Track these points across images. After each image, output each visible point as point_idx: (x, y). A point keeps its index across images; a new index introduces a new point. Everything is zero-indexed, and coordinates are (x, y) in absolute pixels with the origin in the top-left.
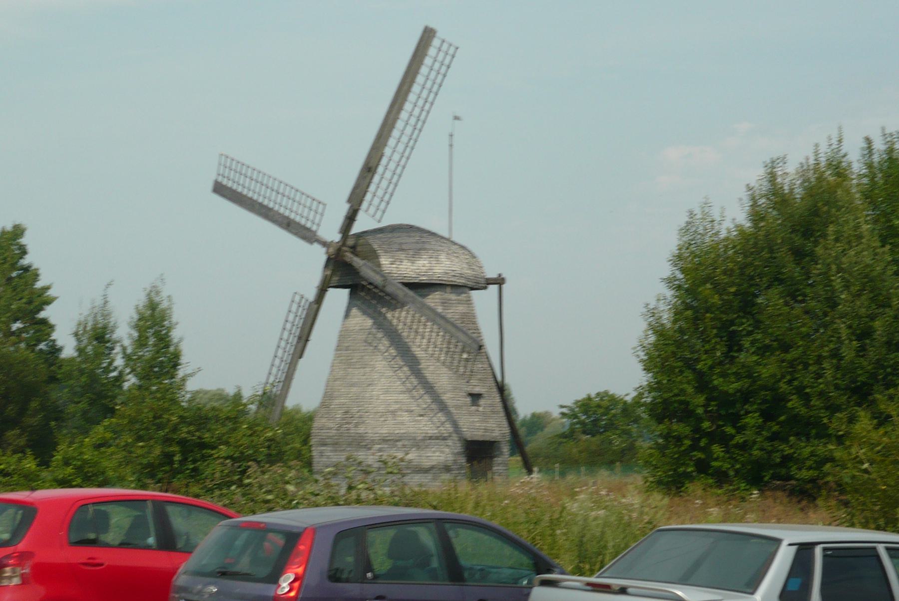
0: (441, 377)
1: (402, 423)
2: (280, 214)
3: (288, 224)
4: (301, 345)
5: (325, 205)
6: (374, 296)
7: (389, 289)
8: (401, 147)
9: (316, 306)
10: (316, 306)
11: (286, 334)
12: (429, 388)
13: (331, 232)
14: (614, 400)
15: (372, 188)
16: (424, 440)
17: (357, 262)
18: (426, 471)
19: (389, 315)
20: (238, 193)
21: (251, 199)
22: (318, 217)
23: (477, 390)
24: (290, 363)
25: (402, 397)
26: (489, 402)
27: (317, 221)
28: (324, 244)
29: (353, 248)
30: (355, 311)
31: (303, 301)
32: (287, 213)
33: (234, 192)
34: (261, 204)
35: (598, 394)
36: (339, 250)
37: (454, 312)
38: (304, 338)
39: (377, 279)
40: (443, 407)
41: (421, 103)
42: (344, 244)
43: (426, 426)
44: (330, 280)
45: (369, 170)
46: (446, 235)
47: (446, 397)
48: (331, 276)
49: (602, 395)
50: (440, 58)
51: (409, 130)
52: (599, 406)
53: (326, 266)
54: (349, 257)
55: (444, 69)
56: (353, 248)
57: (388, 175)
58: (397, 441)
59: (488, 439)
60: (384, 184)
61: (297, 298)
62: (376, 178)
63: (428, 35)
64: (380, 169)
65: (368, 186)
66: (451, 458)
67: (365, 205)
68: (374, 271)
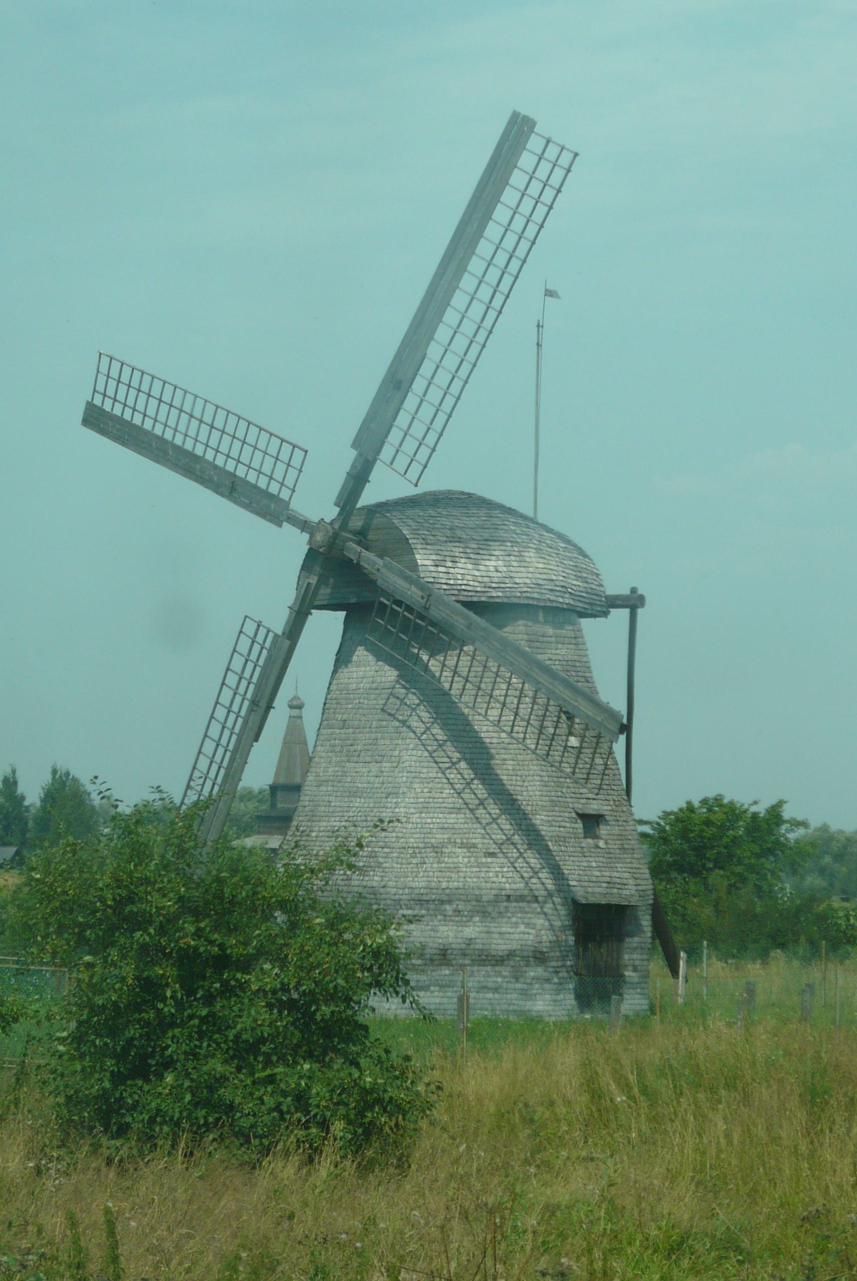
0: (528, 779)
1: (456, 869)
2: (216, 467)
3: (232, 488)
4: (255, 718)
6: (406, 626)
7: (435, 613)
8: (460, 343)
9: (287, 643)
10: (287, 643)
11: (227, 694)
12: (509, 803)
13: (319, 503)
14: (733, 813)
15: (403, 419)
16: (496, 900)
17: (370, 560)
18: (499, 961)
19: (434, 666)
21: (161, 439)
23: (594, 807)
24: (234, 752)
25: (452, 818)
26: (616, 830)
27: (289, 482)
28: (304, 525)
29: (361, 536)
30: (361, 653)
31: (262, 631)
32: (230, 466)
34: (180, 450)
35: (704, 802)
36: (336, 536)
37: (556, 655)
38: (262, 704)
39: (413, 594)
40: (534, 839)
41: (501, 259)
42: (344, 526)
43: (501, 875)
44: (315, 594)
46: (531, 514)
47: (539, 820)
48: (318, 587)
49: (713, 804)
50: (542, 173)
51: (477, 310)
52: (708, 823)
53: (307, 566)
54: (353, 550)
55: (549, 194)
56: (361, 536)
57: (434, 395)
58: (442, 902)
59: (614, 901)
60: (426, 412)
61: (250, 628)
62: (411, 402)
63: (519, 129)
64: (419, 385)
65: (395, 417)
66: (547, 937)
67: (387, 453)
68: (406, 578)
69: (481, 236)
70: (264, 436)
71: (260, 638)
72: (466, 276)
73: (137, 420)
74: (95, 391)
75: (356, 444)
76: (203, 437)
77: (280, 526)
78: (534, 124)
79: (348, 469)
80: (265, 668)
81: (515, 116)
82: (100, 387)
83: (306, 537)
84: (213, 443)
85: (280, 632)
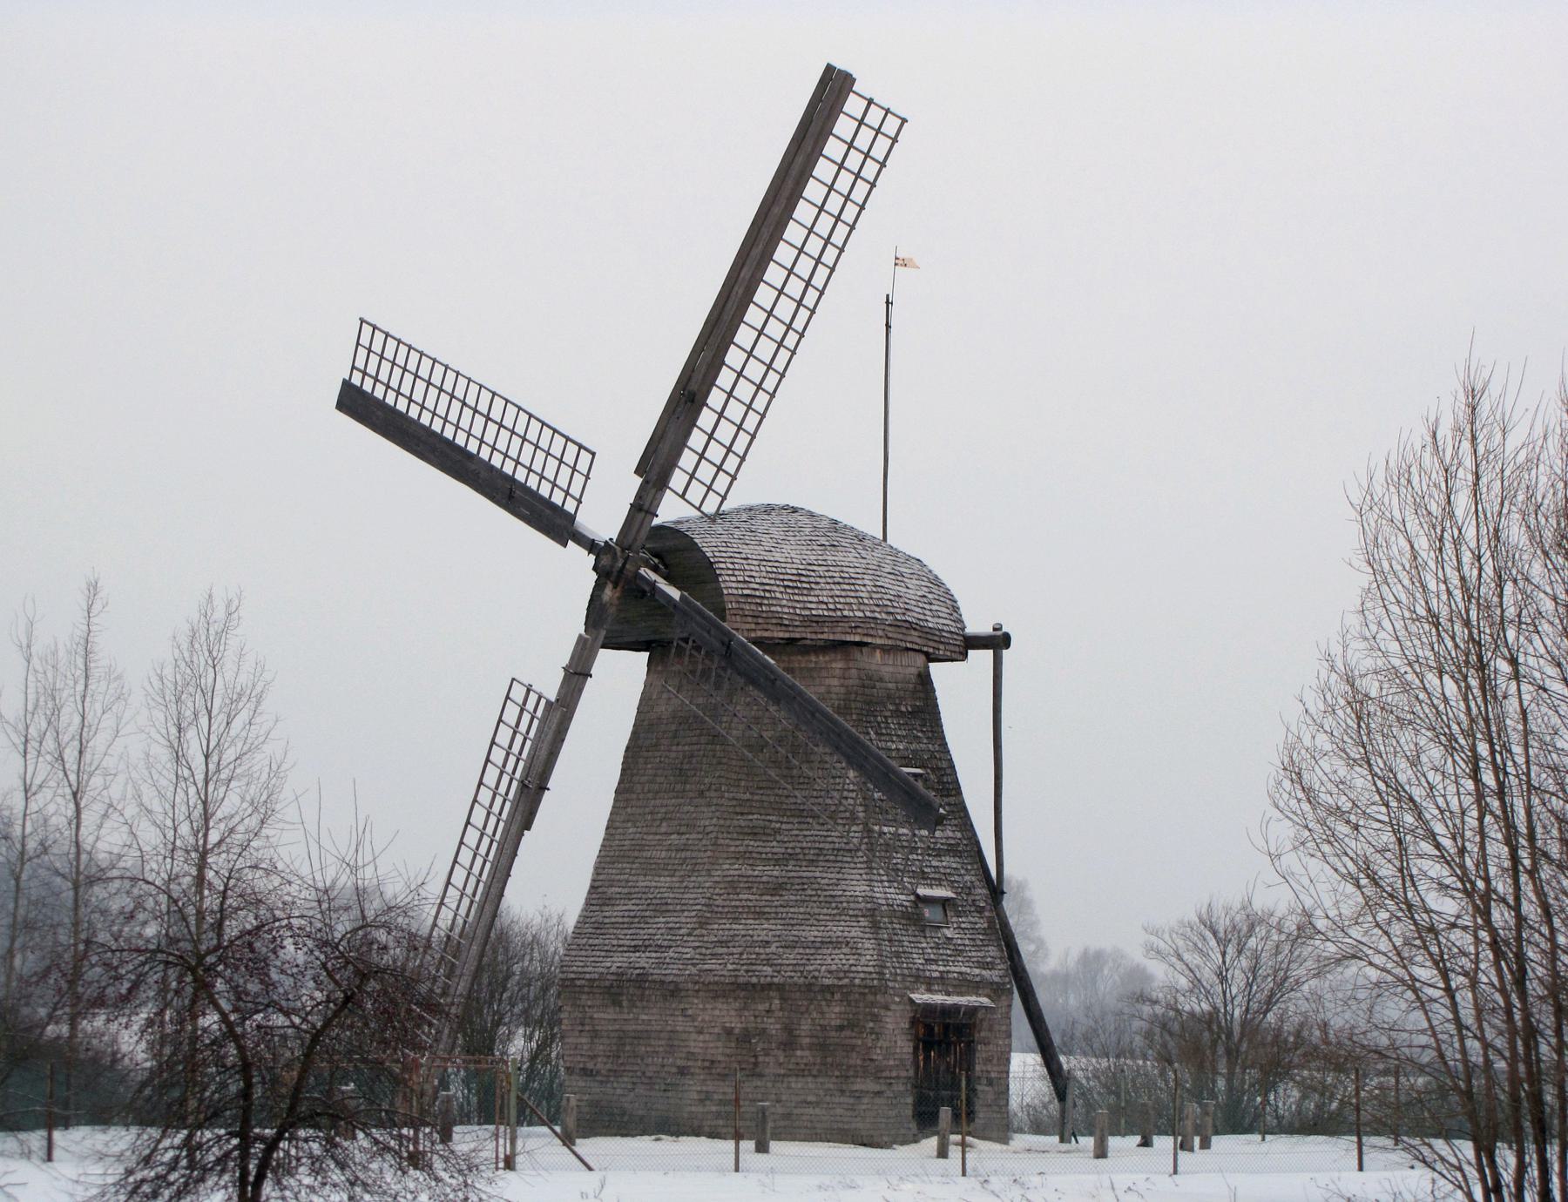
5: (593, 454)
13: (604, 515)
22: (579, 480)
27: (575, 490)
28: (591, 546)
31: (533, 698)
38: (532, 789)
45: (688, 398)
55: (830, 254)
61: (518, 693)
63: (834, 87)
69: (713, 384)
70: (547, 433)
71: (530, 706)
72: (714, 390)
73: (402, 406)
74: (353, 367)
76: (477, 431)
77: (565, 545)
79: (566, 660)
80: (543, 721)
81: (829, 69)
82: (360, 364)
84: (489, 438)
85: (553, 699)
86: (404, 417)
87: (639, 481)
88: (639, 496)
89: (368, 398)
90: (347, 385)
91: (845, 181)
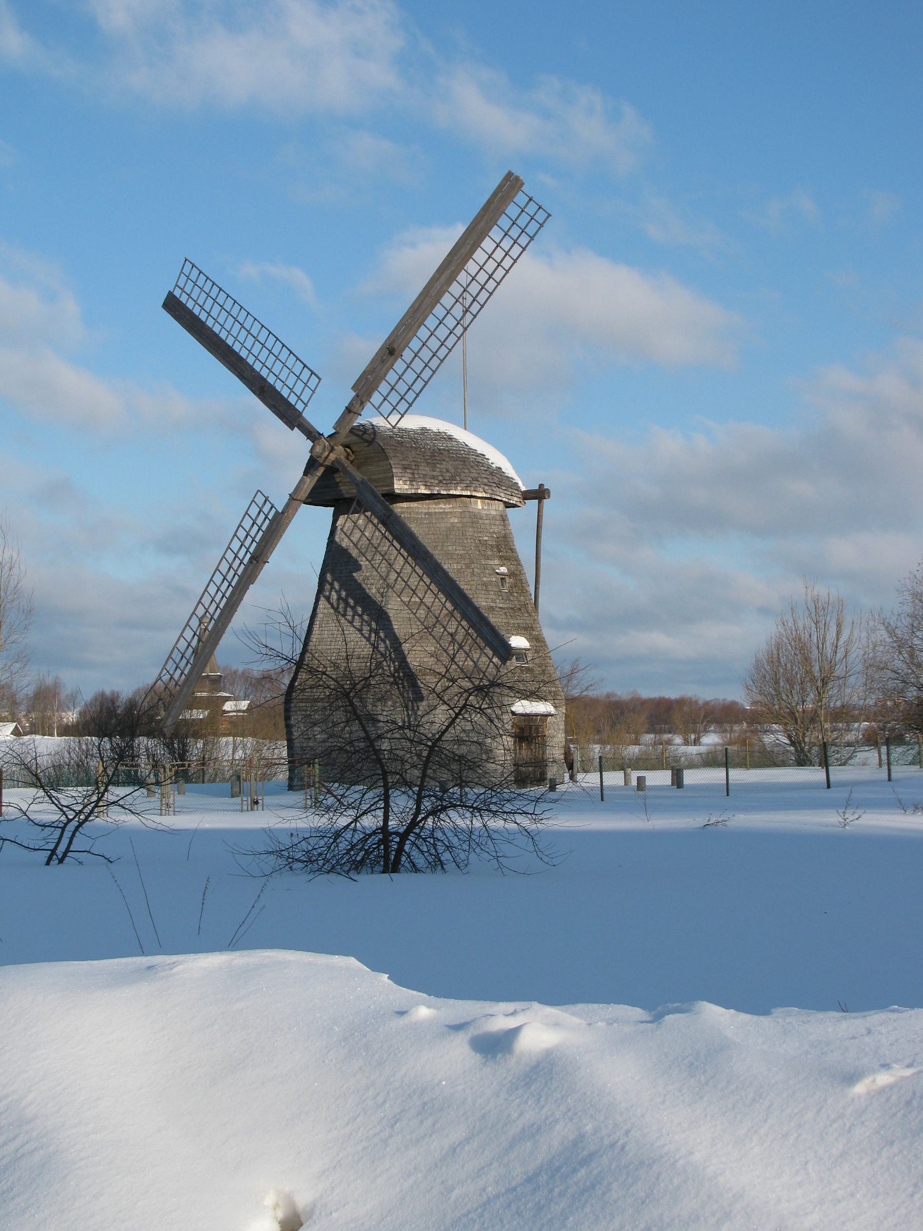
5: (320, 379)
13: (324, 416)
20: (221, 339)
22: (307, 392)
27: (305, 398)
28: (311, 434)
33: (196, 318)
45: (391, 351)
61: (260, 500)
72: (463, 273)
75: (354, 388)
77: (292, 429)
78: (523, 184)
81: (510, 174)
83: (310, 444)
86: (203, 324)
87: (353, 394)
88: (351, 403)
89: (183, 306)
90: (171, 296)
91: (499, 255)
